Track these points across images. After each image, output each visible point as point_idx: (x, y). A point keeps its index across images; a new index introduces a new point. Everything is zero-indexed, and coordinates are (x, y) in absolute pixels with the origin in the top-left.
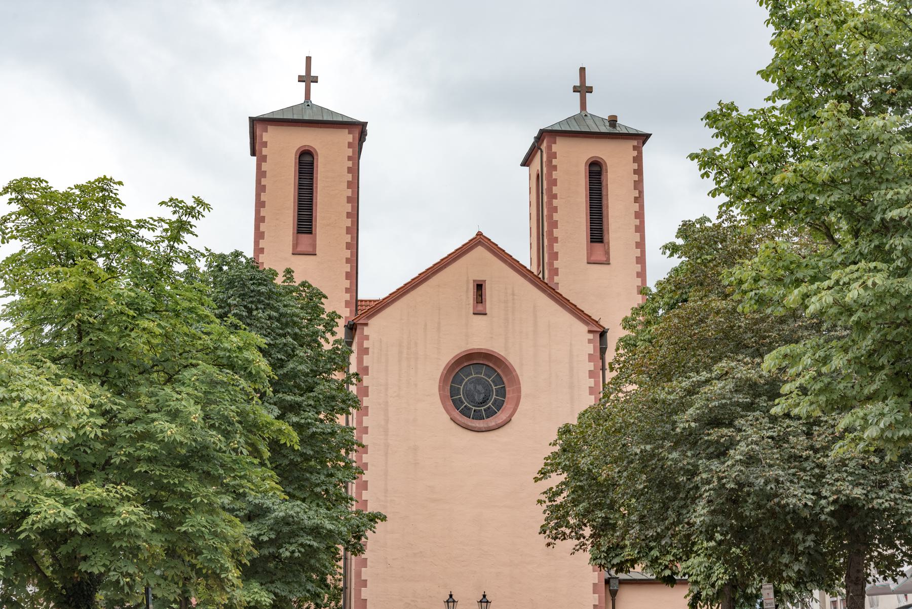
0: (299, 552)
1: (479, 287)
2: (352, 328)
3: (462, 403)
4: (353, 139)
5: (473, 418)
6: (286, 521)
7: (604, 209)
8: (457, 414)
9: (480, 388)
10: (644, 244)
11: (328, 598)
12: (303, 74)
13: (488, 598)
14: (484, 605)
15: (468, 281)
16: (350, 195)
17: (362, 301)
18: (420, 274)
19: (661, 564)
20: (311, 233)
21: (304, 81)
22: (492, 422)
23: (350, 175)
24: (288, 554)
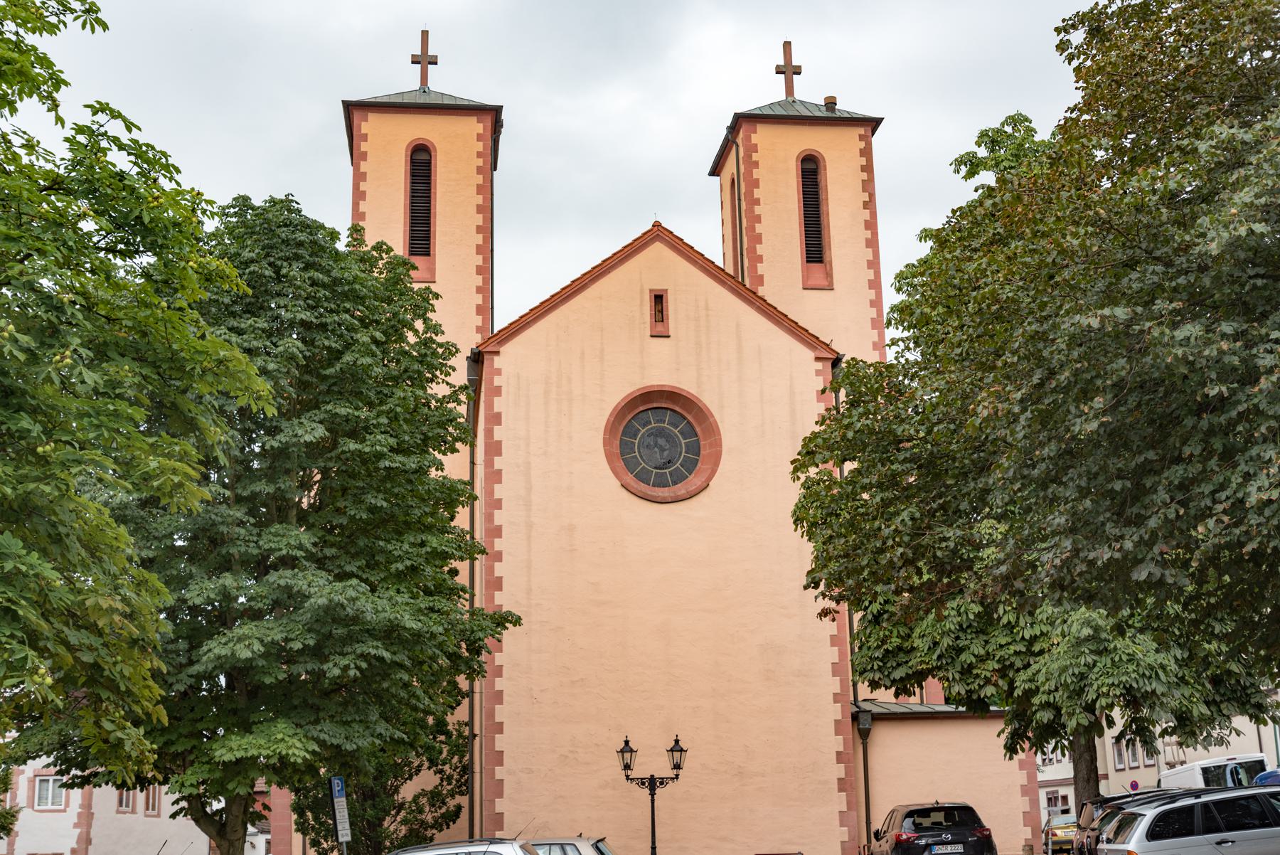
0: (357, 668)
1: (659, 299)
2: (477, 359)
4: (484, 129)
6: (331, 613)
7: (823, 217)
8: (630, 479)
10: (879, 263)
11: (448, 751)
13: (682, 744)
14: (677, 755)
15: (642, 291)
16: (481, 202)
18: (573, 282)
19: (977, 676)
20: (429, 255)
22: (681, 489)
24: (337, 672)
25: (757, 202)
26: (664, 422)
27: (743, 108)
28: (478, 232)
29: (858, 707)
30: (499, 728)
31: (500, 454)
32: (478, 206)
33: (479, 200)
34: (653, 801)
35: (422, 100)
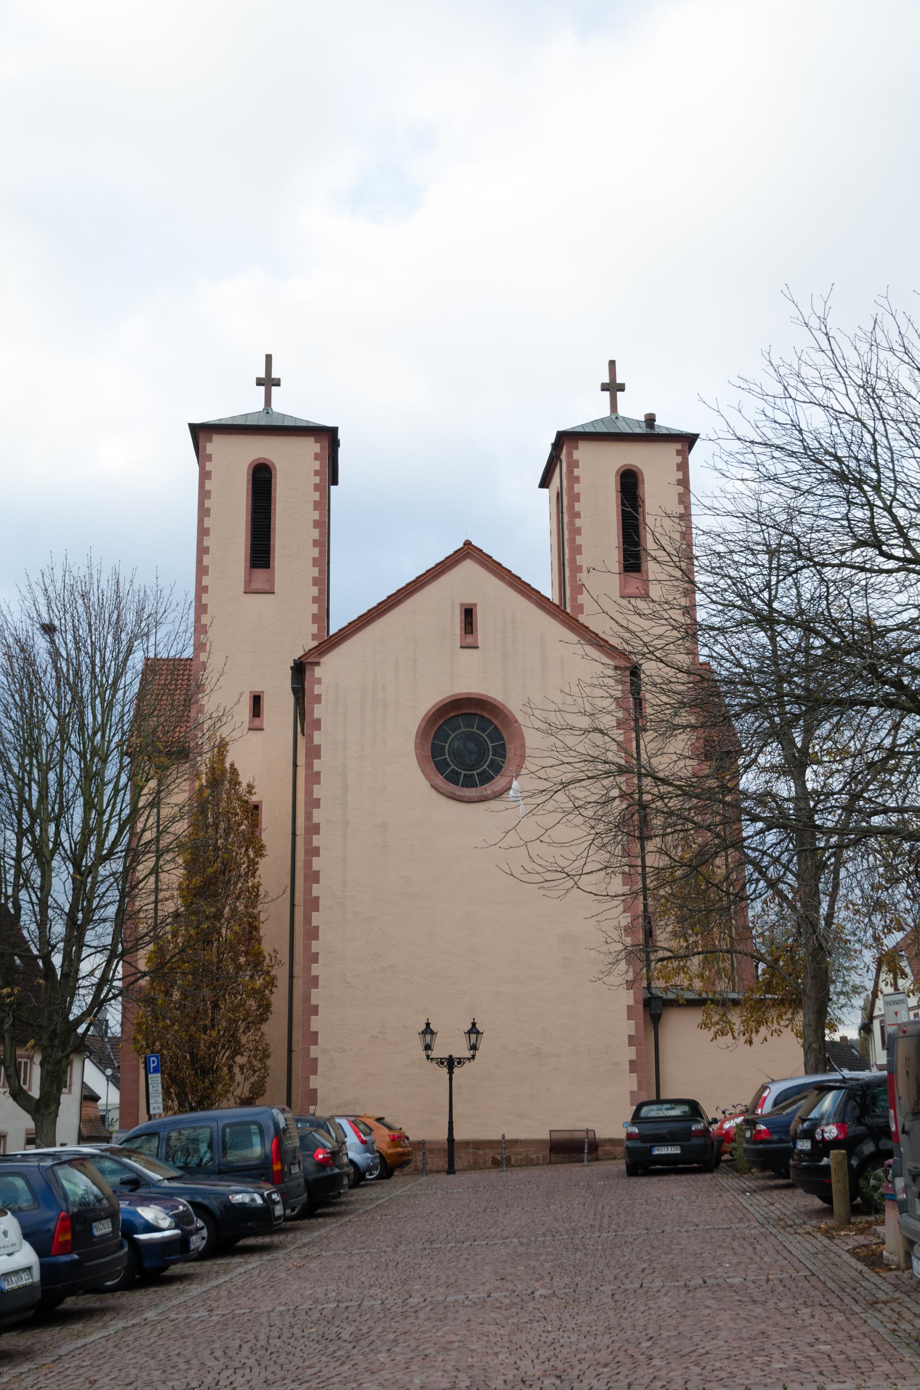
1: (469, 614)
3: (448, 765)
5: (462, 786)
8: (440, 780)
9: (471, 745)
12: (263, 375)
14: (473, 1036)
16: (317, 518)
21: (263, 385)
22: (488, 789)
23: (318, 494)
25: (578, 515)
26: (473, 727)
27: (567, 425)
28: (314, 546)
29: (650, 993)
30: (315, 1010)
31: (319, 757)
32: (315, 521)
33: (316, 515)
34: (451, 1079)
35: (263, 422)
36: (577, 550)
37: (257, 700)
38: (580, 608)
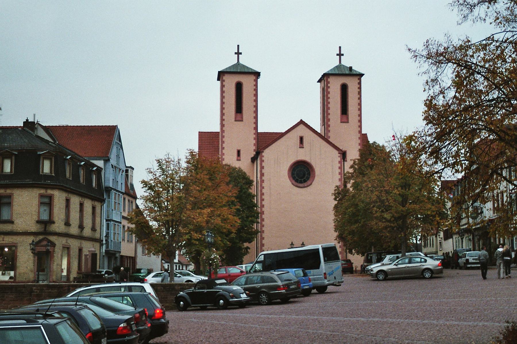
1: (301, 139)
8: (294, 182)
15: (297, 136)
17: (259, 133)
22: (305, 184)
36: (328, 108)
37: (239, 152)
38: (329, 137)
